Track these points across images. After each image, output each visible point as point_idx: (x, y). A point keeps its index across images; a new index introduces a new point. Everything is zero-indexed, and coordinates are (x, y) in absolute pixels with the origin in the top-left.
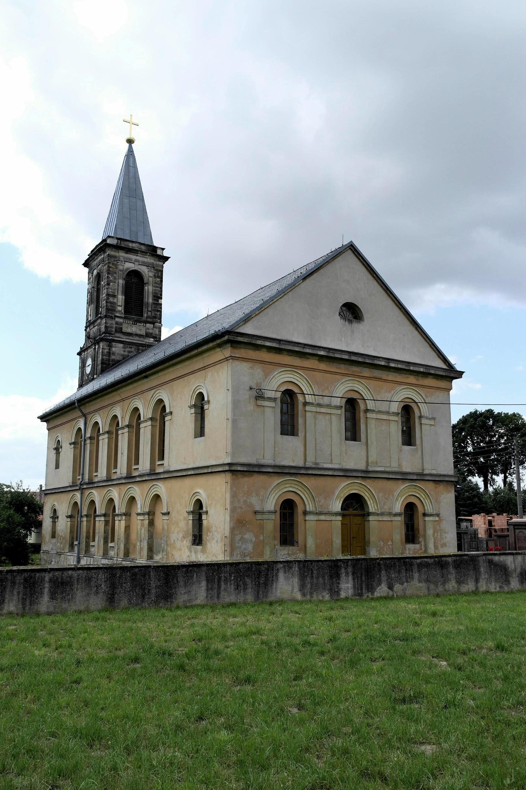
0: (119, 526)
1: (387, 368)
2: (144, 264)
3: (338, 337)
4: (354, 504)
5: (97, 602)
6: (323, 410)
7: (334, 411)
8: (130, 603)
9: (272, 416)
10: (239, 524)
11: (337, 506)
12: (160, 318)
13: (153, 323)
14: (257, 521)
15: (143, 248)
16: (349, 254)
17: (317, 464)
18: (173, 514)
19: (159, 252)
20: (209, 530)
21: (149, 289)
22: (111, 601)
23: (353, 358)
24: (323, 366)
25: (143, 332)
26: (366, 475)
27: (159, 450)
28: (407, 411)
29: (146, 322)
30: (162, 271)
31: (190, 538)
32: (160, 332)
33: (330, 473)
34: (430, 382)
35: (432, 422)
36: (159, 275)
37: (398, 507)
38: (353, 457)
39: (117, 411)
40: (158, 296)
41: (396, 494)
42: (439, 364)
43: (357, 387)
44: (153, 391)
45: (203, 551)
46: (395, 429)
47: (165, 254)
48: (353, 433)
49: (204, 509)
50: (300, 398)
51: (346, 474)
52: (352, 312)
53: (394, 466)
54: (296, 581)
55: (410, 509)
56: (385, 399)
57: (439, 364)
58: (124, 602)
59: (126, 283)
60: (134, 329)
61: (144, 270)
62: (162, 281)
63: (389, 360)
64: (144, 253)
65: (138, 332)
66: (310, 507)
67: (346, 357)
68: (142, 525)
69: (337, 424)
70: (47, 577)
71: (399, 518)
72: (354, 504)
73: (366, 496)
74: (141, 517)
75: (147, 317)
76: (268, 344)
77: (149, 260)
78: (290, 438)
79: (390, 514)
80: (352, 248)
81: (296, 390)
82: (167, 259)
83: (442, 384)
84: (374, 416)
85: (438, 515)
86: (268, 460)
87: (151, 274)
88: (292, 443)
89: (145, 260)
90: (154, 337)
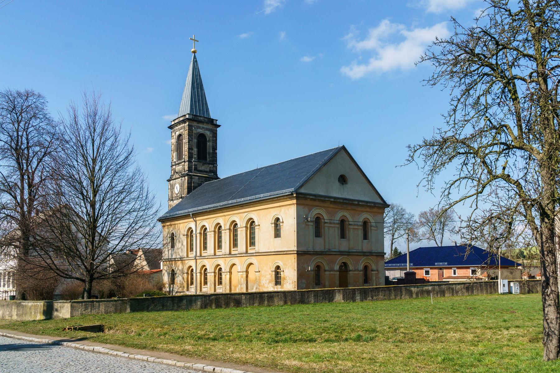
0: (226, 278)
1: (358, 205)
2: (207, 129)
3: (337, 192)
4: (344, 268)
5: (282, 303)
6: (332, 225)
7: (336, 226)
8: (291, 304)
9: (311, 229)
10: (301, 276)
11: (337, 267)
12: (216, 161)
13: (213, 164)
14: (239, 273)
15: (206, 120)
16: (343, 152)
17: (329, 249)
18: (263, 272)
19: (215, 122)
20: (284, 279)
21: (209, 144)
22: (285, 303)
23: (345, 201)
24: (332, 206)
25: (208, 170)
26: (349, 253)
27: (252, 241)
28: (365, 224)
29: (209, 164)
30: (216, 134)
31: (274, 282)
32: (216, 169)
33: (335, 253)
34: (375, 210)
35: (376, 229)
36: (215, 135)
37: (361, 267)
38: (344, 245)
39: (221, 221)
40: (215, 148)
41: (361, 262)
42: (379, 201)
43: (346, 214)
44: (246, 214)
45: (281, 288)
46: (360, 233)
47: (218, 123)
48: (343, 235)
49: (282, 270)
50: (323, 220)
51: (341, 253)
52: (343, 180)
53: (360, 249)
54: (341, 296)
55: (366, 268)
56: (356, 219)
57: (379, 201)
58: (289, 303)
59: (198, 140)
60: (202, 168)
61: (208, 134)
62: (216, 139)
63: (359, 201)
64: (207, 123)
65: (205, 170)
66: (327, 268)
67: (342, 201)
68: (242, 277)
69: (336, 232)
70: (266, 295)
71: (362, 272)
72: (344, 268)
73: (349, 263)
74: (241, 273)
75: (210, 161)
76: (311, 197)
77: (210, 127)
78: (319, 238)
79: (358, 270)
80: (344, 148)
81: (321, 217)
82: (219, 126)
83: (381, 211)
84: (352, 227)
85: (377, 270)
86: (311, 249)
87: (211, 135)
88: (319, 241)
89: (208, 127)
90: (213, 173)
